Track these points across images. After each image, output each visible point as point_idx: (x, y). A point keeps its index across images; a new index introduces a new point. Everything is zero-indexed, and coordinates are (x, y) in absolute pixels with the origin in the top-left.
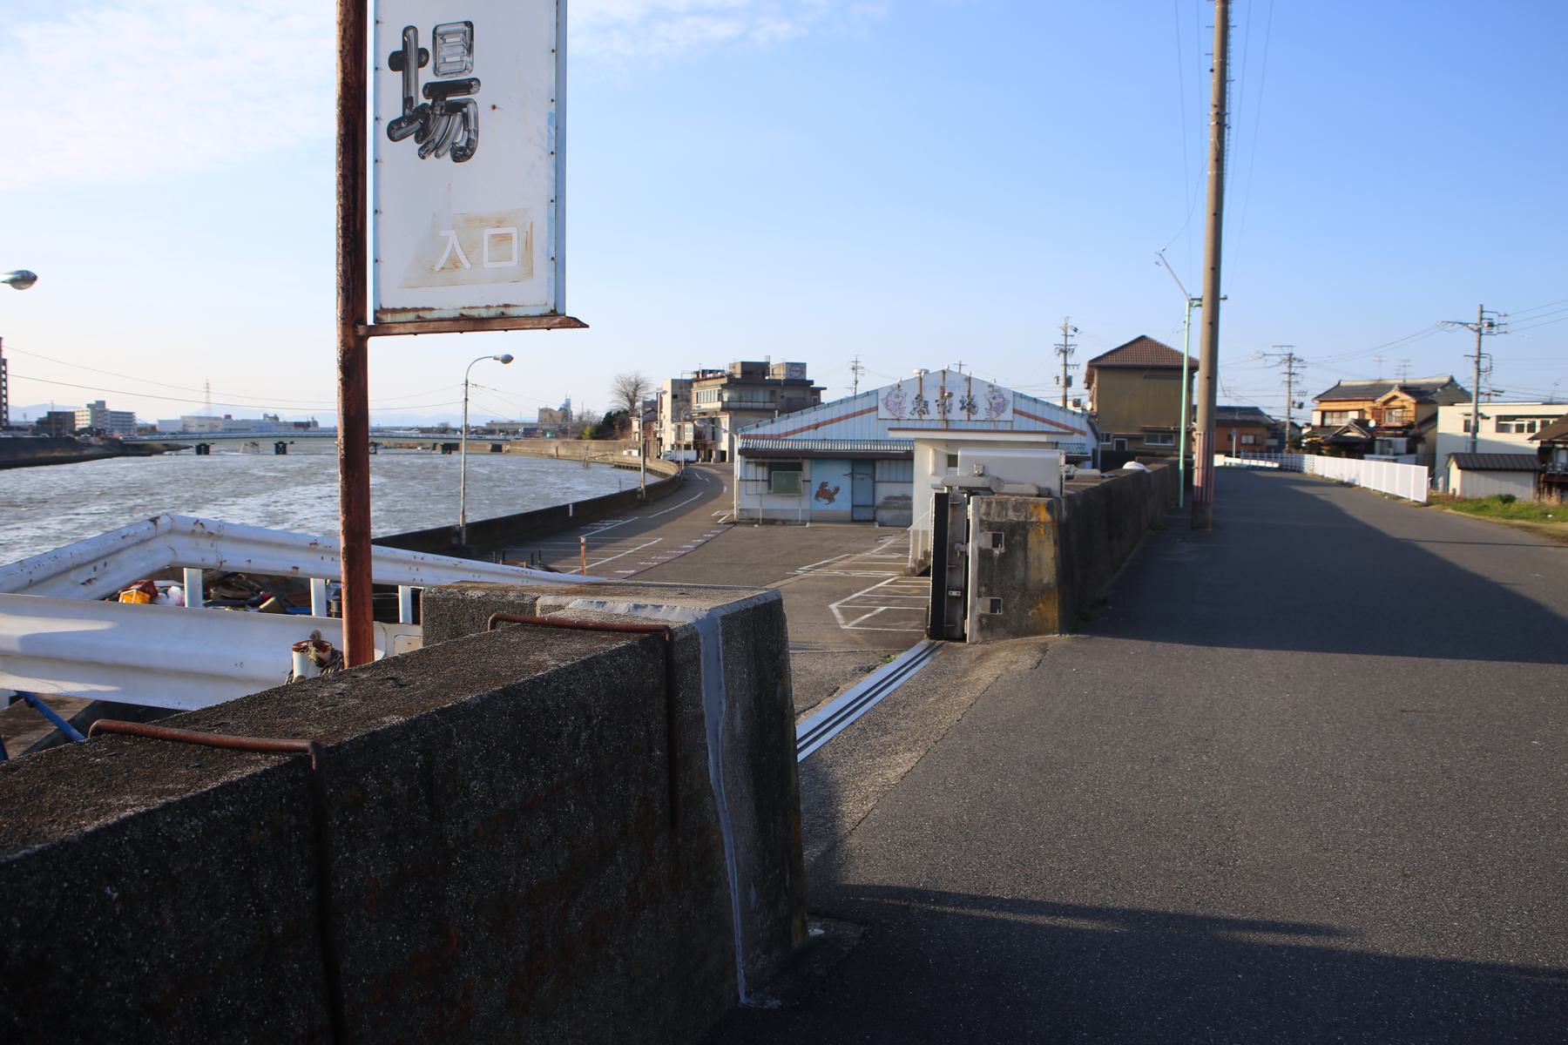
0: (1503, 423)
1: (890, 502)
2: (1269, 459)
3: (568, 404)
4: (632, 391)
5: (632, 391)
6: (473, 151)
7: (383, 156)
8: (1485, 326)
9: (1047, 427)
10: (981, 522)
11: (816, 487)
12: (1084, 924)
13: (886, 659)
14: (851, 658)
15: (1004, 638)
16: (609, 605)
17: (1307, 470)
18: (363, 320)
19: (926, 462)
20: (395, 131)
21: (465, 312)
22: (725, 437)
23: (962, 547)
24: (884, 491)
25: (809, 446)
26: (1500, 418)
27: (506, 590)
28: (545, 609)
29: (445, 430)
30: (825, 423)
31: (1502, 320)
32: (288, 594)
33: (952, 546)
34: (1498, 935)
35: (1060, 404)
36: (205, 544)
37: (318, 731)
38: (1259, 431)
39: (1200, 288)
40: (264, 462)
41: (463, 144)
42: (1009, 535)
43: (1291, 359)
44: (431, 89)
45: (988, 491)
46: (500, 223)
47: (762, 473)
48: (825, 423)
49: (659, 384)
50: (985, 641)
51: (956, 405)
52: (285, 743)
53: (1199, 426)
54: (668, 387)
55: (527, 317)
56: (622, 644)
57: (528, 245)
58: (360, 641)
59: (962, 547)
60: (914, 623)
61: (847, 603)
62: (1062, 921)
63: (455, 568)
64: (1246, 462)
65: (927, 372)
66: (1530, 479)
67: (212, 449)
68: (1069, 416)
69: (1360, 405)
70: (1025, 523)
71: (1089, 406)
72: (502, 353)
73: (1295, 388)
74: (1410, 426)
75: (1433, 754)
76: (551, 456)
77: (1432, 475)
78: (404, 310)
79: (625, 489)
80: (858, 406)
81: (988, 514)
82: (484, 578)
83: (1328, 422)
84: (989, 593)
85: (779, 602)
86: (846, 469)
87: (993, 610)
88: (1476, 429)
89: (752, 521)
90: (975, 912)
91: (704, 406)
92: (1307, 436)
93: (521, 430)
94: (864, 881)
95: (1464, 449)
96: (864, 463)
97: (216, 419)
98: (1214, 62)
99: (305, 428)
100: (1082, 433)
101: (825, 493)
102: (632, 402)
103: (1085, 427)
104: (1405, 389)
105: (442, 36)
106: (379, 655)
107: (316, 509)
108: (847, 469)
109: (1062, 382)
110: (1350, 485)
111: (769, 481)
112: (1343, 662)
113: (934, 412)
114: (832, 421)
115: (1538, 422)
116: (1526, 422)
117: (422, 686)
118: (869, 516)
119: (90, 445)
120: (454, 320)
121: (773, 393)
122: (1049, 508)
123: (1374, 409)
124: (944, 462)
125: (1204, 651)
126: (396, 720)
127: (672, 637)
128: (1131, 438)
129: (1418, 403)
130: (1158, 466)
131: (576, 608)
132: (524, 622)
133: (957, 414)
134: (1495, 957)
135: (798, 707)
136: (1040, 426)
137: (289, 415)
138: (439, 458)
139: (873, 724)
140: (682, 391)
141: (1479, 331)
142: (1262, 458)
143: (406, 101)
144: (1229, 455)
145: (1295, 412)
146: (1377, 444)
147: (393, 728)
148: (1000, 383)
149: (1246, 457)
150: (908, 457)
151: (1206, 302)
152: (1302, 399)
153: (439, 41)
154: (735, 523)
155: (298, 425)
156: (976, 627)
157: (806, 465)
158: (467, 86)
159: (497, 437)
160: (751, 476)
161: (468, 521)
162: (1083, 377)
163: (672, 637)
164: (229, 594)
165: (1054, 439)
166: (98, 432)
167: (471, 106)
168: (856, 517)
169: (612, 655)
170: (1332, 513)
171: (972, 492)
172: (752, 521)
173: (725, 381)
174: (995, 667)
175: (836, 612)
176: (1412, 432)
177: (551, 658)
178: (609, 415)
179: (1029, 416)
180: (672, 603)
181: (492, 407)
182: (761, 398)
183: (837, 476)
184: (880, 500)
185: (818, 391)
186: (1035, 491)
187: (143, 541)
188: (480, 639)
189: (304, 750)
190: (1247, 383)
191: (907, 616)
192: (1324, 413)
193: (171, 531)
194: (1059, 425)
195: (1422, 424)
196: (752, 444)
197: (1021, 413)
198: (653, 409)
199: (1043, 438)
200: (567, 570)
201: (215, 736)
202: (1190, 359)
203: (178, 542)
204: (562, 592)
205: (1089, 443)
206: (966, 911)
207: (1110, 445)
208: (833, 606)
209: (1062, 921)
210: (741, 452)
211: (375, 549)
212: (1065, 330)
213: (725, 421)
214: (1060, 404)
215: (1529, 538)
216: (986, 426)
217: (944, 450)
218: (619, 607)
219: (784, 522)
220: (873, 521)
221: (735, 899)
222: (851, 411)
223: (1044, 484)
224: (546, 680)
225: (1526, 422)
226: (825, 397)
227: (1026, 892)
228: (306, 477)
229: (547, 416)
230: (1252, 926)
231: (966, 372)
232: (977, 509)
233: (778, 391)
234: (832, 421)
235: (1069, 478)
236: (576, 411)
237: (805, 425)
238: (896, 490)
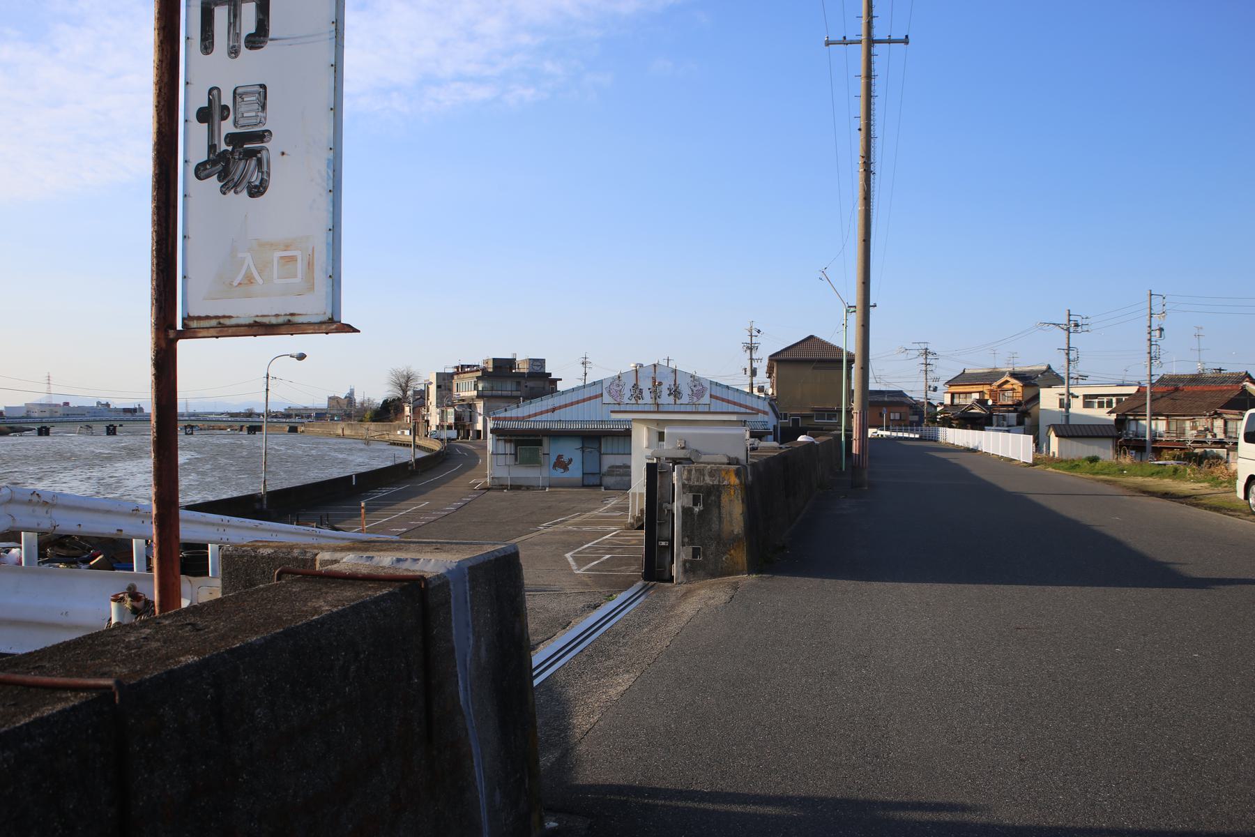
0: (1088, 401)
1: (613, 470)
2: (912, 431)
3: (352, 393)
4: (405, 382)
5: (405, 382)
7: (191, 192)
8: (1072, 326)
9: (737, 409)
10: (684, 486)
11: (553, 459)
12: (770, 810)
13: (609, 598)
14: (581, 598)
15: (705, 578)
16: (376, 559)
17: (941, 439)
18: (174, 326)
19: (642, 438)
20: (201, 171)
21: (258, 320)
22: (480, 419)
23: (669, 506)
24: (609, 461)
25: (547, 426)
26: (1085, 396)
27: (292, 547)
28: (324, 563)
29: (250, 414)
30: (560, 407)
31: (1085, 321)
32: (115, 553)
33: (661, 505)
34: (1093, 805)
35: (748, 390)
36: (40, 511)
37: (122, 670)
38: (904, 409)
39: (854, 298)
40: (100, 443)
41: (257, 183)
42: (707, 495)
43: (926, 352)
44: (231, 138)
45: (689, 460)
46: (287, 247)
47: (509, 448)
48: (560, 407)
49: (426, 376)
50: (689, 582)
51: (665, 392)
52: (92, 682)
53: (856, 406)
54: (433, 379)
55: (309, 324)
56: (385, 591)
57: (310, 265)
58: (169, 592)
59: (669, 506)
60: (633, 568)
61: (579, 552)
62: (751, 809)
63: (256, 528)
64: (894, 434)
65: (641, 366)
66: (1109, 443)
67: (52, 430)
68: (755, 400)
69: (980, 388)
70: (719, 486)
71: (770, 392)
72: (296, 352)
73: (930, 375)
74: (1019, 404)
75: (1041, 662)
76: (338, 436)
77: (1037, 442)
78: (208, 318)
79: (398, 461)
81: (689, 479)
82: (274, 538)
83: (956, 401)
84: (691, 542)
85: (516, 554)
86: (577, 444)
87: (694, 556)
88: (1069, 406)
89: (502, 487)
90: (681, 804)
91: (462, 394)
92: (941, 412)
93: (313, 414)
94: (591, 781)
95: (1060, 421)
96: (592, 439)
97: (56, 405)
99: (132, 413)
100: (765, 413)
101: (561, 464)
102: (405, 392)
103: (767, 409)
104: (1014, 375)
105: (241, 95)
106: (185, 603)
107: (138, 478)
108: (578, 444)
109: (749, 373)
110: (974, 451)
111: (516, 454)
112: (971, 591)
113: (647, 398)
114: (566, 406)
115: (1114, 399)
116: (1105, 400)
117: (216, 630)
118: (598, 482)
120: (249, 326)
121: (518, 383)
122: (738, 473)
123: (991, 391)
124: (656, 438)
125: (863, 585)
126: (191, 659)
127: (426, 585)
128: (804, 417)
129: (1024, 386)
131: (349, 561)
132: (305, 575)
133: (666, 399)
134: (1092, 823)
135: (534, 639)
136: (731, 408)
137: (118, 403)
138: (245, 439)
139: (599, 651)
140: (445, 382)
141: (1068, 330)
142: (906, 431)
143: (211, 150)
144: (879, 427)
145: (931, 394)
146: (994, 418)
147: (188, 666)
148: (699, 374)
149: (894, 431)
150: (627, 434)
152: (936, 384)
154: (488, 489)
155: (126, 410)
156: (681, 570)
157: (545, 441)
158: (261, 136)
159: (293, 420)
161: (269, 489)
163: (426, 585)
164: (63, 553)
165: (743, 418)
167: (264, 153)
168: (586, 483)
169: (376, 601)
170: (960, 473)
171: (676, 461)
172: (502, 487)
173: (479, 374)
174: (697, 602)
175: (570, 559)
176: (1020, 409)
177: (325, 604)
178: (385, 402)
179: (723, 400)
180: (428, 556)
181: (287, 396)
182: (509, 387)
183: (571, 451)
184: (605, 468)
185: (555, 381)
186: (726, 461)
188: (267, 589)
189: (109, 687)
190: (892, 372)
191: (627, 562)
192: (953, 395)
194: (746, 407)
195: (1028, 402)
196: (501, 424)
197: (717, 398)
198: (421, 397)
199: (734, 418)
200: (350, 529)
201: (32, 678)
202: (848, 354)
203: (15, 509)
204: (336, 549)
205: (770, 421)
206: (673, 803)
207: (788, 422)
208: (568, 555)
209: (751, 809)
211: (183, 514)
212: (751, 331)
213: (480, 406)
214: (748, 390)
215: (1110, 489)
216: (689, 409)
217: (655, 428)
218: (385, 561)
219: (528, 488)
220: (600, 485)
221: (483, 801)
222: (580, 398)
223: (732, 455)
224: (321, 622)
225: (1105, 400)
226: (561, 386)
227: (723, 785)
228: (132, 453)
229: (334, 403)
230: (902, 806)
231: (672, 365)
233: (523, 382)
234: (566, 406)
235: (753, 449)
236: (358, 398)
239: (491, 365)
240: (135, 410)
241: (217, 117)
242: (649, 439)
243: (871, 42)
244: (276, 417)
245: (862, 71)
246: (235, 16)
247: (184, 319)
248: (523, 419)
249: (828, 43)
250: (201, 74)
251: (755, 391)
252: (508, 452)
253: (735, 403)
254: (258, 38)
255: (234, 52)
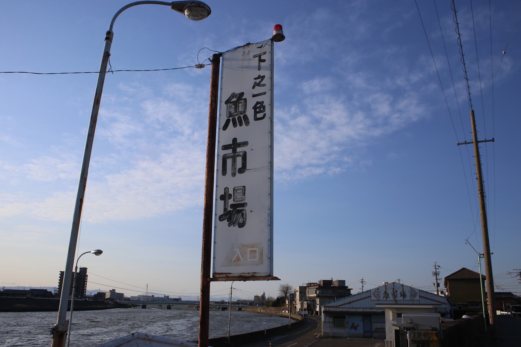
6: (245, 225)
10: (412, 340)
11: (350, 325)
19: (390, 315)
20: (221, 218)
22: (318, 306)
25: (348, 310)
29: (223, 302)
30: (353, 302)
43: (458, 144)
44: (232, 206)
46: (253, 247)
47: (331, 320)
48: (353, 302)
49: (295, 287)
51: (399, 295)
54: (298, 289)
55: (261, 277)
57: (261, 254)
65: (387, 283)
71: (447, 294)
78: (222, 273)
80: (364, 296)
81: (414, 337)
91: (310, 295)
98: (477, 176)
100: (445, 304)
101: (354, 327)
102: (286, 294)
103: (446, 302)
105: (236, 190)
109: (436, 285)
111: (334, 322)
113: (391, 297)
119: (109, 304)
120: (238, 277)
122: (437, 335)
124: (396, 316)
130: (475, 316)
133: (399, 298)
137: (173, 295)
140: (303, 290)
150: (383, 314)
151: (485, 255)
153: (235, 192)
154: (322, 338)
155: (175, 299)
158: (244, 205)
160: (327, 321)
162: (444, 283)
166: (112, 300)
167: (244, 211)
171: (408, 329)
173: (317, 287)
178: (278, 298)
179: (425, 298)
183: (358, 321)
184: (373, 329)
186: (430, 329)
187: (129, 341)
193: (138, 338)
194: (436, 301)
197: (423, 297)
198: (293, 296)
199: (431, 307)
202: (482, 275)
205: (447, 307)
210: (324, 312)
213: (318, 301)
214: (436, 293)
216: (410, 302)
219: (340, 337)
220: (371, 337)
222: (362, 297)
226: (353, 292)
231: (401, 282)
232: (410, 335)
234: (355, 301)
235: (443, 322)
236: (267, 297)
237: (346, 302)
238: (379, 326)
239: (322, 283)
240: (178, 299)
241: (227, 198)
242: (393, 316)
243: (477, 142)
244: (233, 304)
245: (475, 154)
246: (234, 162)
247: (213, 274)
248: (336, 307)
249: (458, 144)
250: (221, 183)
251: (439, 293)
252: (331, 321)
253: (431, 300)
254: (243, 170)
255: (234, 175)
